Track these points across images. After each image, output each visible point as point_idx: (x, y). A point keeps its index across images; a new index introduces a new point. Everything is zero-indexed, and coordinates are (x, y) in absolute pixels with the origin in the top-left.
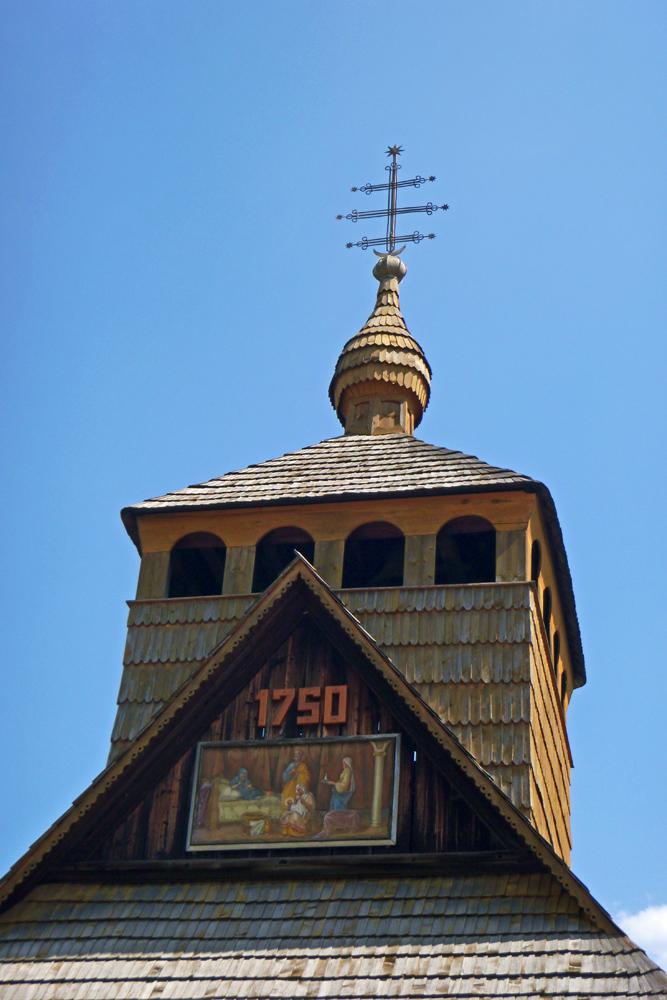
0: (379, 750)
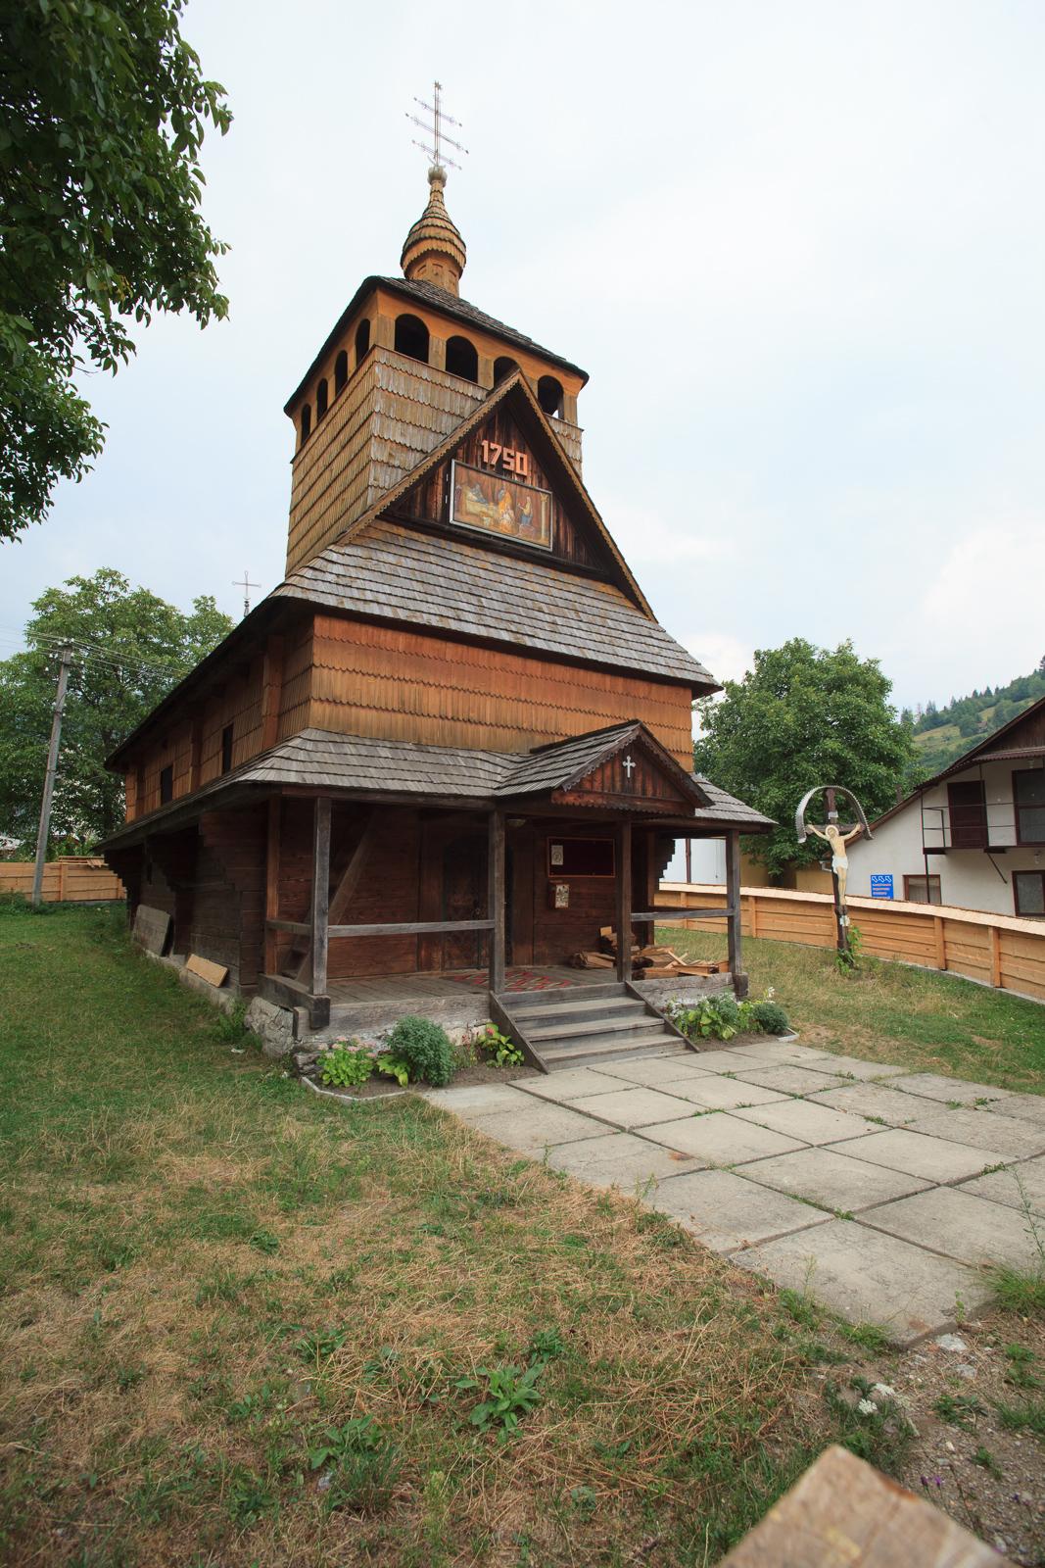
0: (544, 498)
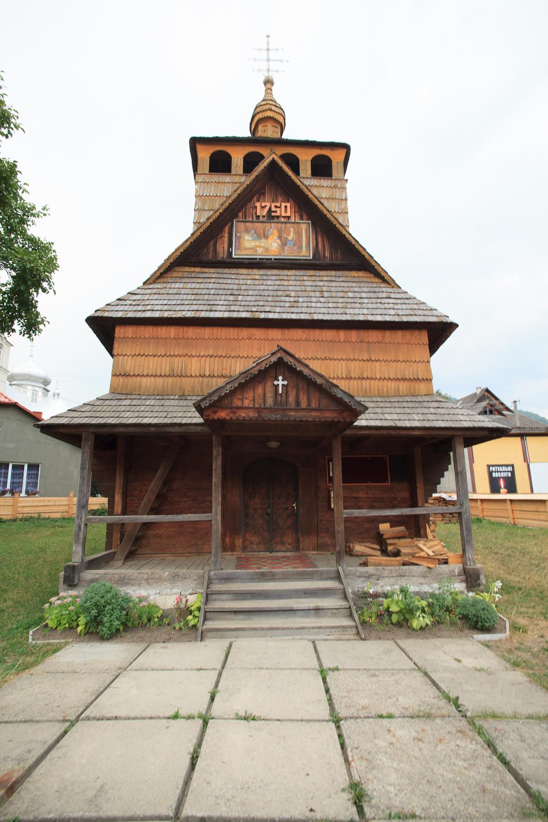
0: (304, 227)
